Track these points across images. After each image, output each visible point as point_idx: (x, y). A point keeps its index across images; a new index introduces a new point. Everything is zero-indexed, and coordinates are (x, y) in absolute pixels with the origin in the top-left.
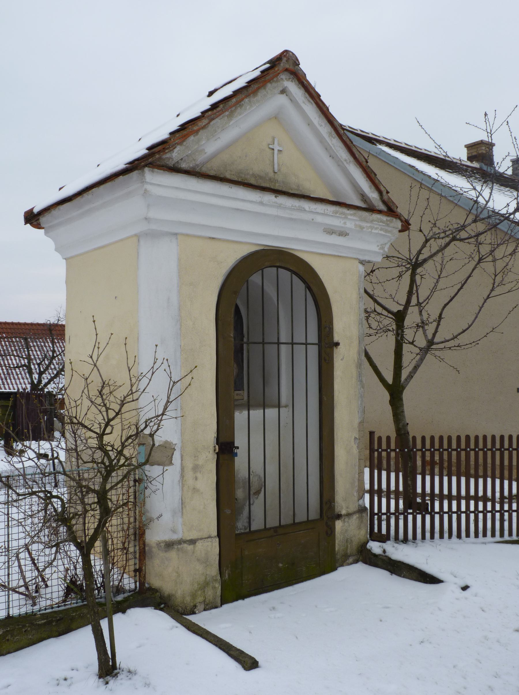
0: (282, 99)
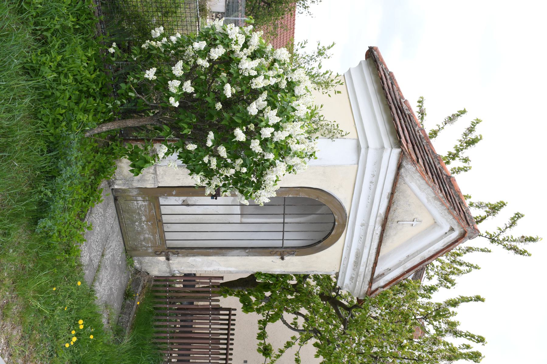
0: (447, 228)
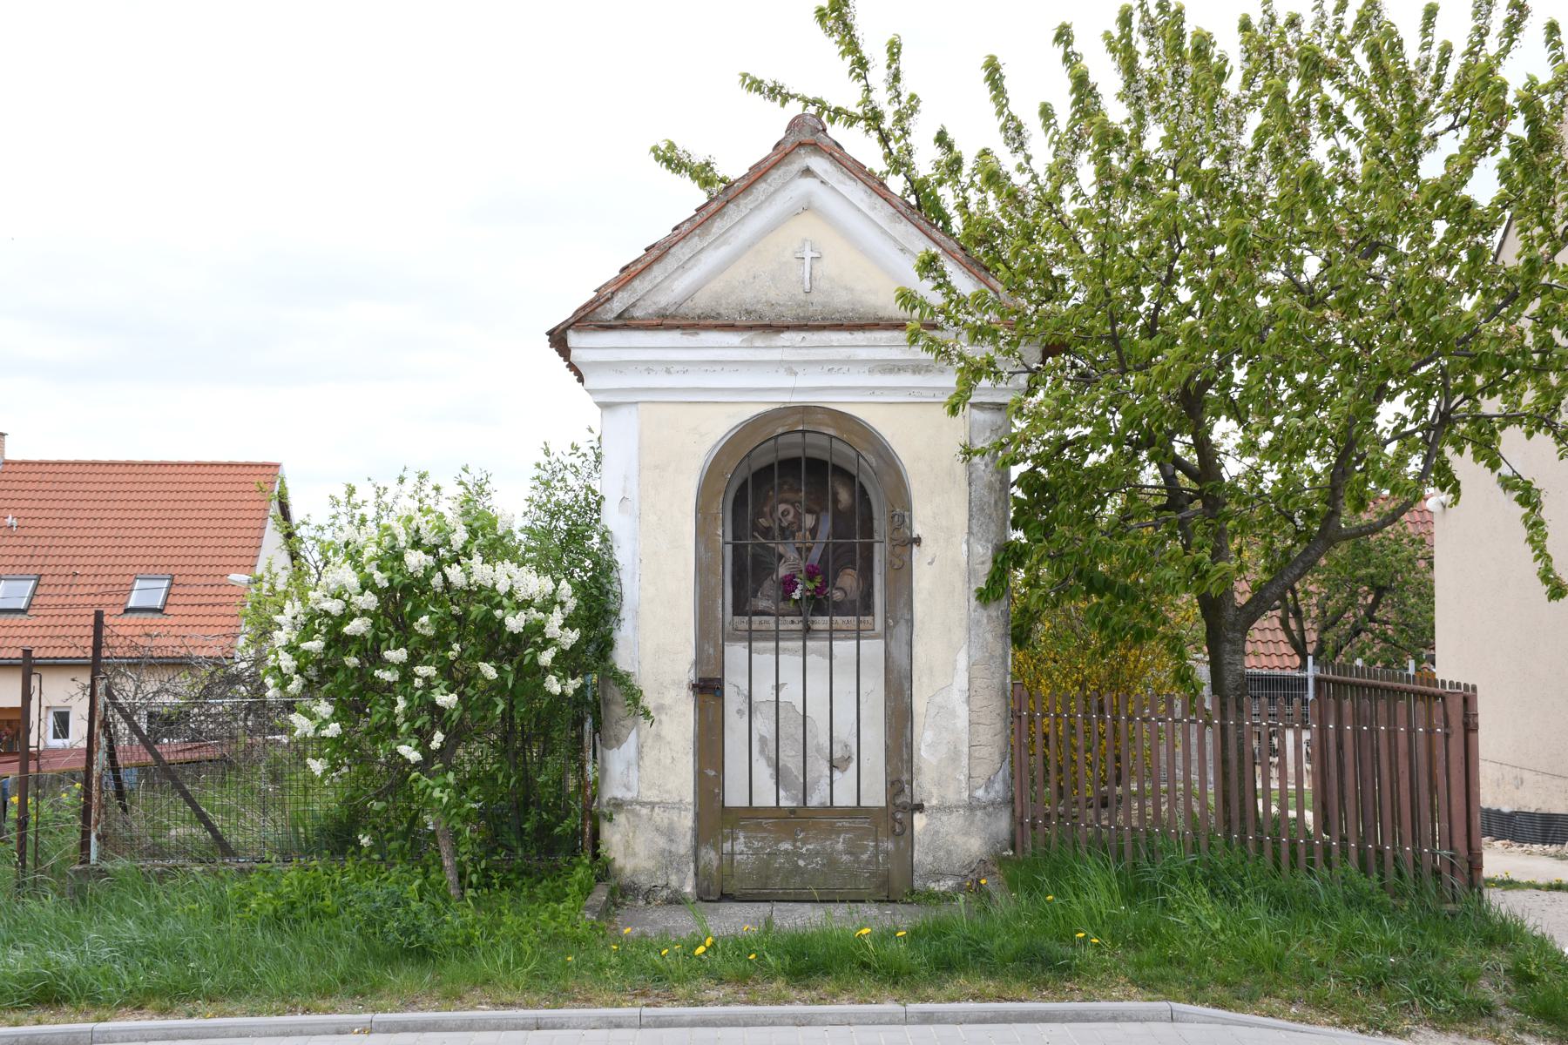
0: (808, 184)
